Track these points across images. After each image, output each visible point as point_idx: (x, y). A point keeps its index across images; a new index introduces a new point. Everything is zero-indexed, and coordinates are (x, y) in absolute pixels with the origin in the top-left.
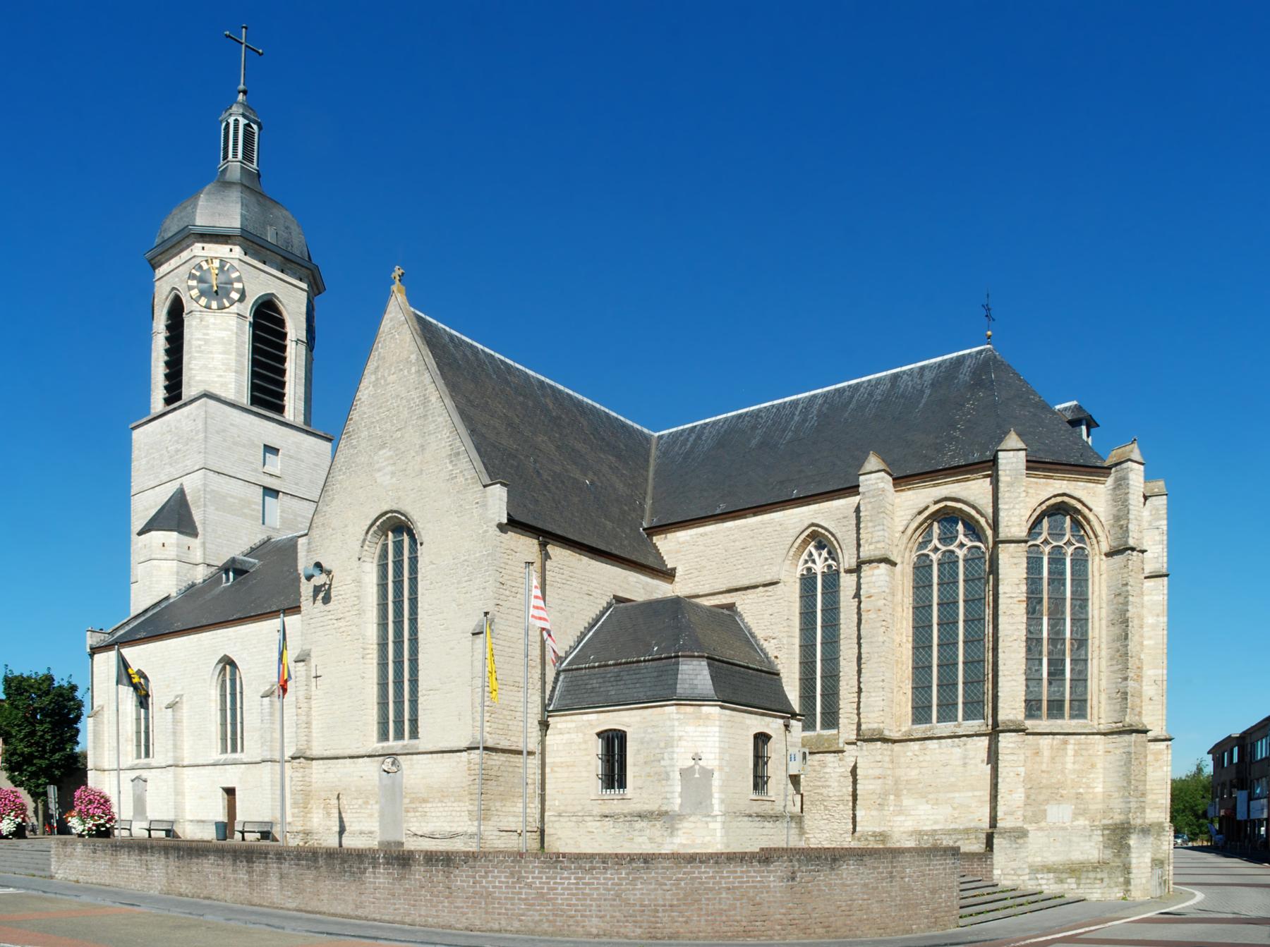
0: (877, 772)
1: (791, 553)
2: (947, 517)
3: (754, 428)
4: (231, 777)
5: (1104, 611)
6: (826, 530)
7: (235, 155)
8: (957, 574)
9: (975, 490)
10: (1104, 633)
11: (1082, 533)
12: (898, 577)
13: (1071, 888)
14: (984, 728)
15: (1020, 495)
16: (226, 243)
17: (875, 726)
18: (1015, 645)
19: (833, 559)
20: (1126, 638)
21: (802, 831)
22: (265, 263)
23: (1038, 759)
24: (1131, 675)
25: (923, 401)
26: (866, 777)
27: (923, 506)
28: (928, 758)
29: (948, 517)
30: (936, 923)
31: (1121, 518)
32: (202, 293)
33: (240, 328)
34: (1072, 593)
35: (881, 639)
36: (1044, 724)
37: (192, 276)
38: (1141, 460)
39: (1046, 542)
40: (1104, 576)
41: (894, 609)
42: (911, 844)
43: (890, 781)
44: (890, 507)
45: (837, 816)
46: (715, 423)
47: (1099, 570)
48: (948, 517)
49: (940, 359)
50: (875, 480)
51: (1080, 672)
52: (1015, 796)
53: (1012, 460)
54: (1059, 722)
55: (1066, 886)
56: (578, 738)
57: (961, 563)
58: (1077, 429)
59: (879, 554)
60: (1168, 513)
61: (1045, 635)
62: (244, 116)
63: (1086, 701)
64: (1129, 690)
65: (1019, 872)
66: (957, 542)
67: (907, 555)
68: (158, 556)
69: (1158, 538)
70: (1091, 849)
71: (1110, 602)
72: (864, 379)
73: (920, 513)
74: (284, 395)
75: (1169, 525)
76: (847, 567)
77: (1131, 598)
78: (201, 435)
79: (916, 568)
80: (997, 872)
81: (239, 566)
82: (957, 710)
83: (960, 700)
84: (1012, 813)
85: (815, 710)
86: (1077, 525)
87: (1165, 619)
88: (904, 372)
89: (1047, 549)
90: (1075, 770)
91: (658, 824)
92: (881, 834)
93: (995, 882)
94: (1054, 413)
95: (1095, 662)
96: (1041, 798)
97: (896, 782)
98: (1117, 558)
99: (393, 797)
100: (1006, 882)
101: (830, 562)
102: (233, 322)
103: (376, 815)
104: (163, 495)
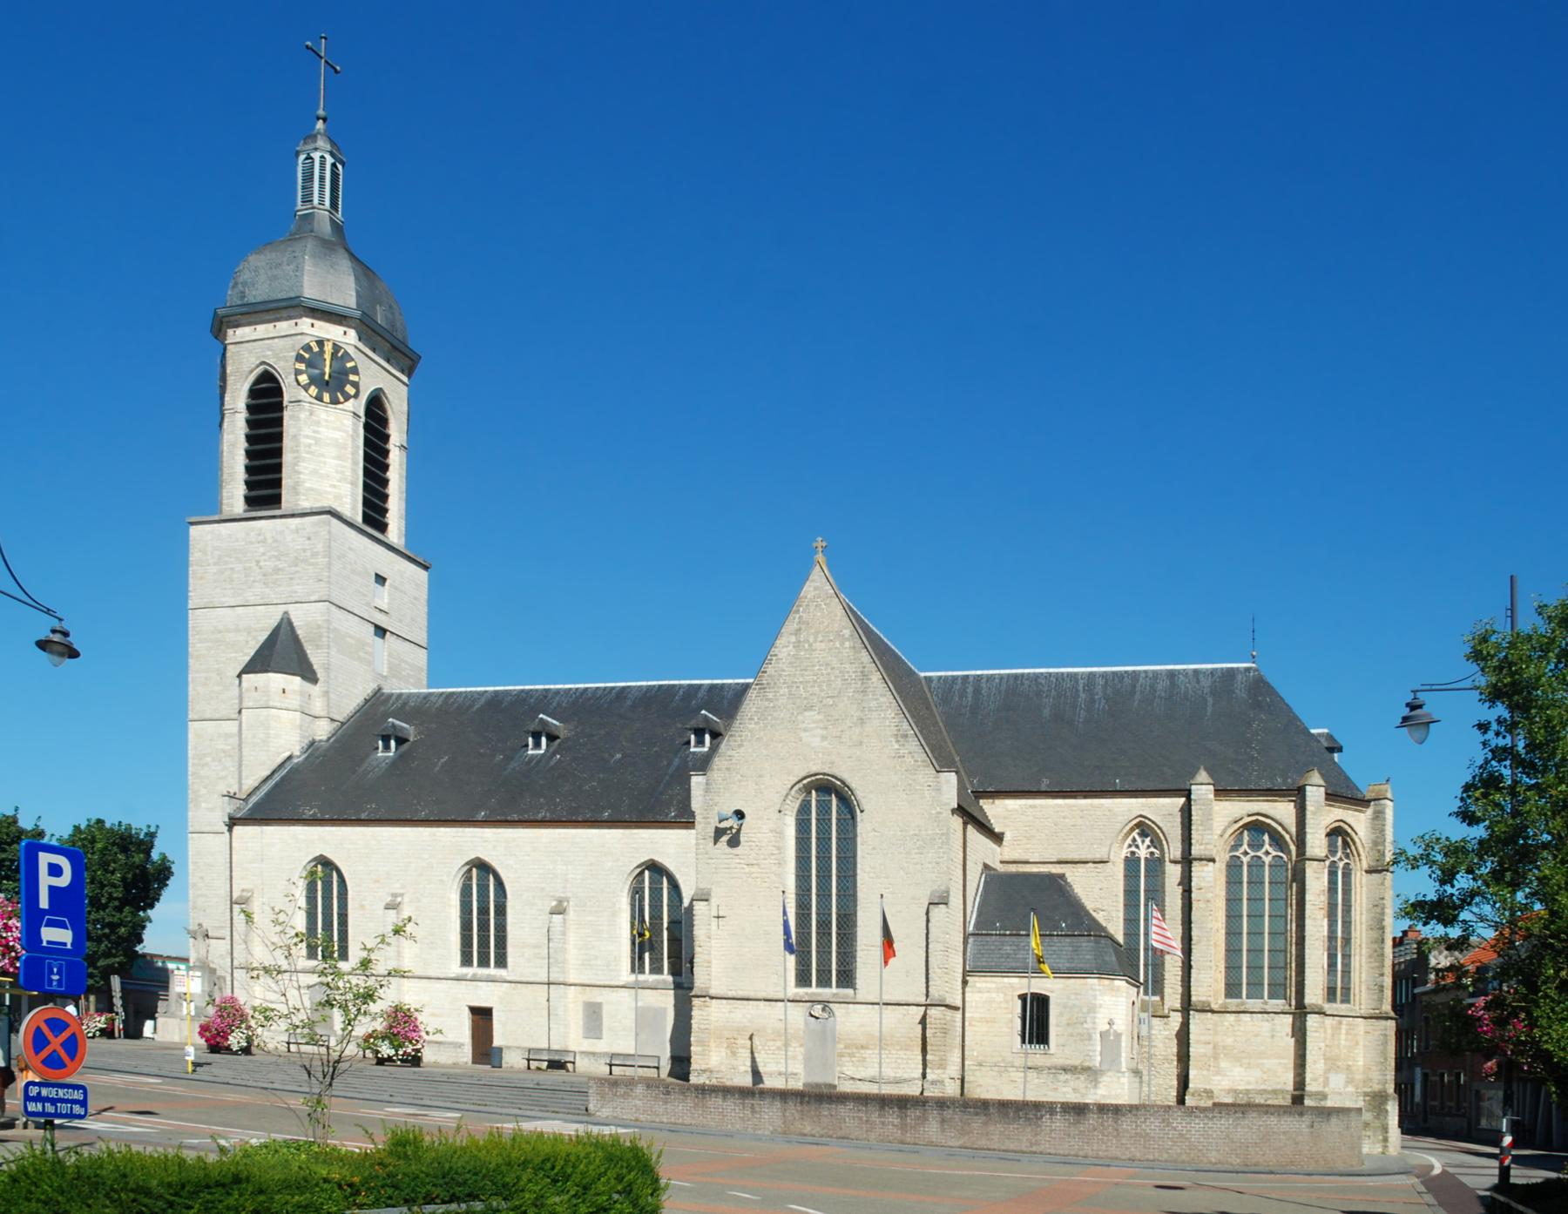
2: (1256, 828)
4: (483, 996)
9: (1282, 811)
16: (340, 324)
22: (374, 350)
26: (1198, 1042)
27: (1238, 816)
33: (355, 431)
37: (299, 358)
42: (1229, 1100)
56: (1000, 998)
62: (332, 154)
71: (1368, 911)
74: (386, 511)
78: (322, 560)
79: (1229, 866)
86: (1346, 844)
91: (1082, 1078)
98: (1375, 876)
99: (823, 1041)
102: (348, 421)
103: (800, 1057)
104: (262, 624)
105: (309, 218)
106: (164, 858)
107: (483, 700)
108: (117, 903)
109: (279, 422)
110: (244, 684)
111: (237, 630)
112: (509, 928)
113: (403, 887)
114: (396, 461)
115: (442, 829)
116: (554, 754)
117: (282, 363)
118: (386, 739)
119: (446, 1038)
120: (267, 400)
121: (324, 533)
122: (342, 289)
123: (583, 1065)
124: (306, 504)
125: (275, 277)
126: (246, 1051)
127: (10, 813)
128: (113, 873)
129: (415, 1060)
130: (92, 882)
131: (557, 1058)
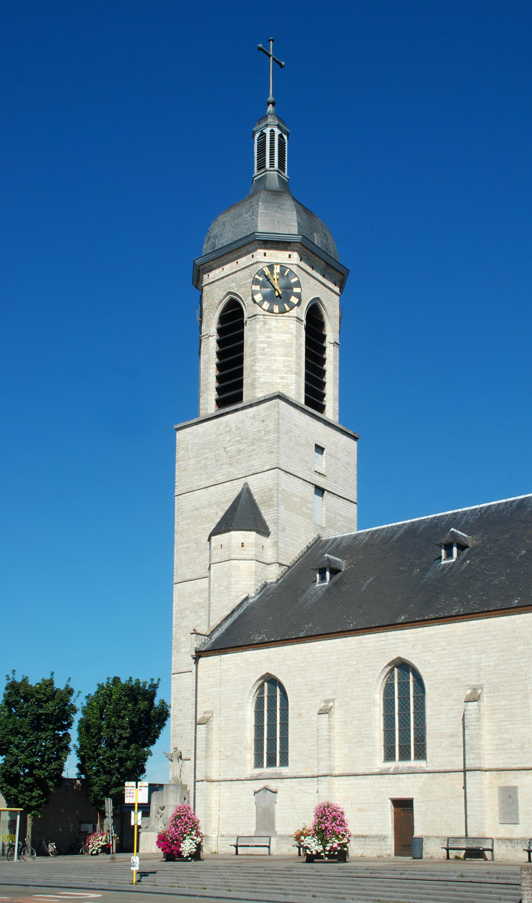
7: (272, 165)
16: (286, 249)
32: (265, 297)
33: (298, 332)
37: (255, 282)
62: (279, 127)
68: (238, 557)
74: (324, 395)
78: (272, 436)
81: (334, 566)
104: (225, 497)
105: (262, 180)
106: (163, 702)
107: (402, 530)
108: (125, 742)
109: (241, 337)
110: (213, 545)
111: (210, 505)
112: (428, 720)
113: (334, 693)
114: (331, 354)
115: (368, 636)
116: (464, 560)
117: (243, 290)
118: (322, 572)
119: (370, 831)
120: (233, 320)
121: (274, 414)
122: (286, 221)
123: (501, 852)
124: (260, 395)
125: (237, 225)
126: (196, 856)
127: (48, 677)
128: (123, 718)
129: (340, 855)
130: (108, 727)
131: (475, 846)
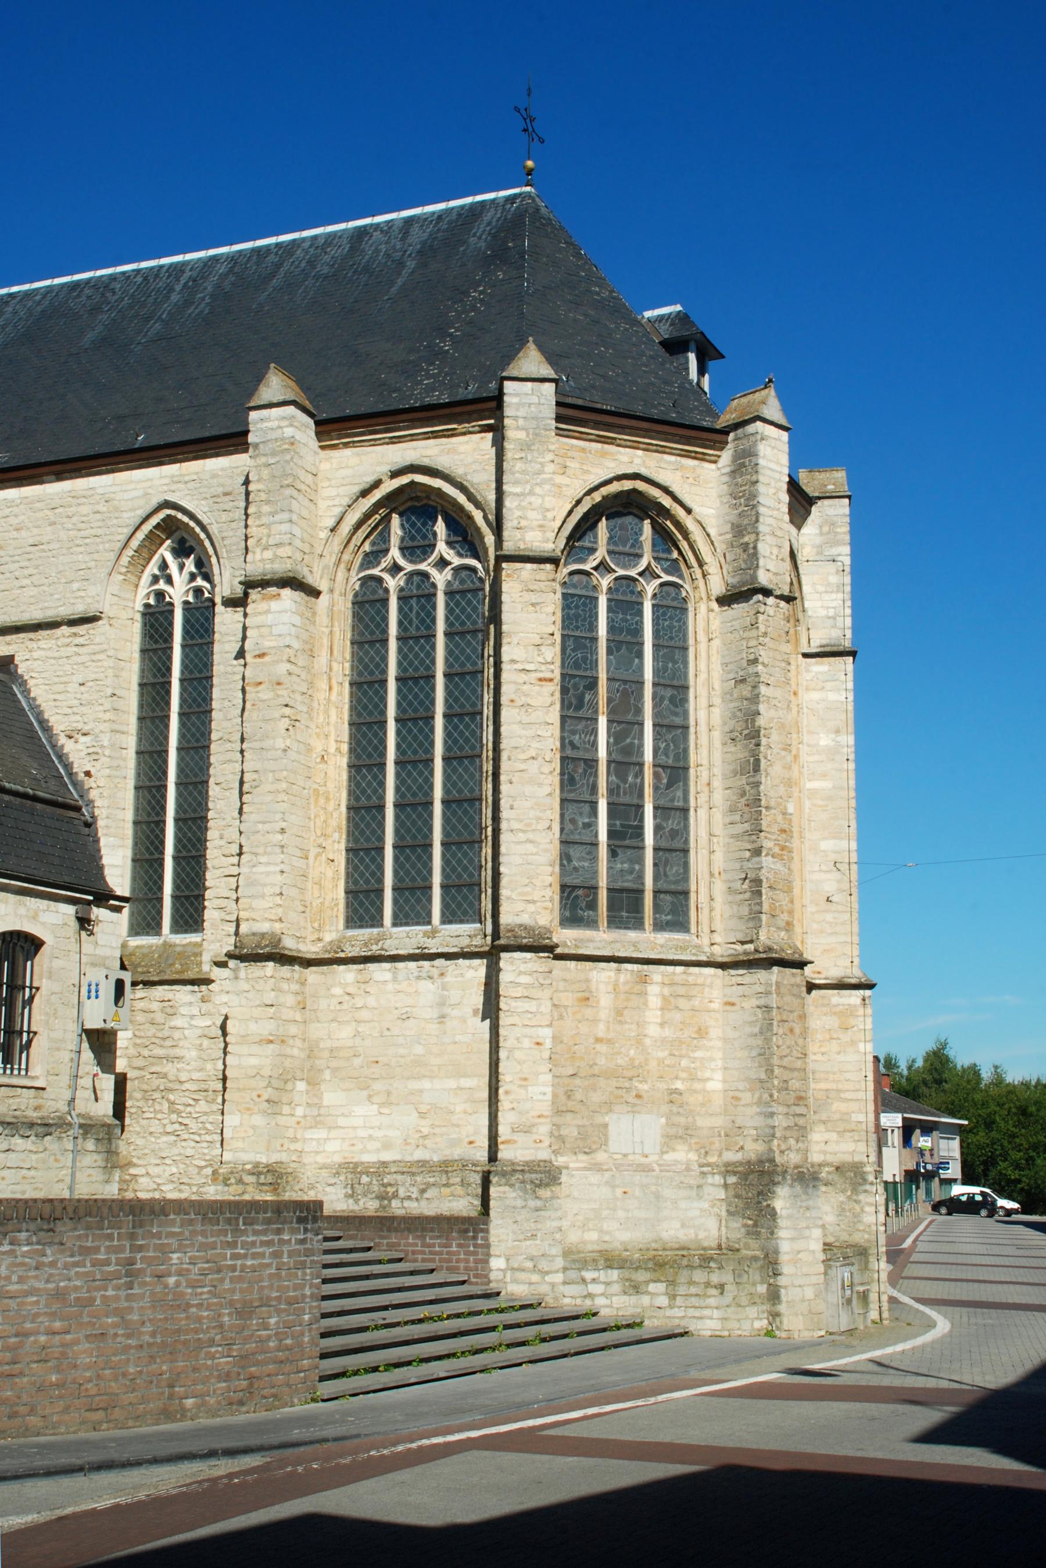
0: (266, 1028)
1: (125, 560)
3: (96, 310)
5: (716, 712)
6: (192, 516)
8: (434, 620)
9: (461, 455)
10: (717, 756)
11: (675, 555)
12: (323, 619)
13: (655, 1305)
14: (478, 941)
15: (539, 471)
17: (264, 927)
18: (533, 767)
19: (207, 577)
20: (757, 769)
21: (112, 1161)
23: (588, 1012)
24: (767, 844)
25: (400, 282)
26: (244, 1039)
27: (370, 479)
28: (371, 1001)
29: (417, 505)
30: (250, 1390)
31: (744, 529)
34: (656, 672)
35: (280, 743)
36: (601, 938)
38: (783, 421)
39: (602, 567)
40: (716, 643)
41: (311, 684)
43: (296, 1050)
44: (309, 479)
45: (193, 1126)
46: (27, 294)
47: (707, 631)
48: (417, 505)
49: (441, 206)
50: (279, 423)
51: (674, 834)
52: (534, 1091)
53: (529, 399)
54: (632, 935)
55: (646, 1300)
57: (441, 600)
58: (676, 361)
59: (281, 569)
60: (853, 532)
61: (602, 753)
63: (686, 893)
64: (764, 874)
65: (544, 1265)
66: (435, 556)
67: (341, 575)
69: (834, 579)
70: (700, 1217)
71: (727, 695)
72: (306, 234)
73: (364, 493)
75: (853, 555)
76: (227, 593)
77: (763, 689)
80: (497, 1264)
82: (430, 900)
83: (437, 879)
84: (527, 1130)
85: (161, 889)
86: (665, 539)
87: (851, 740)
88: (377, 227)
89: (605, 582)
90: (664, 1040)
92: (270, 1169)
93: (493, 1286)
94: (638, 323)
95: (702, 813)
96: (596, 1097)
97: (312, 1052)
100: (516, 1289)
101: (200, 582)
